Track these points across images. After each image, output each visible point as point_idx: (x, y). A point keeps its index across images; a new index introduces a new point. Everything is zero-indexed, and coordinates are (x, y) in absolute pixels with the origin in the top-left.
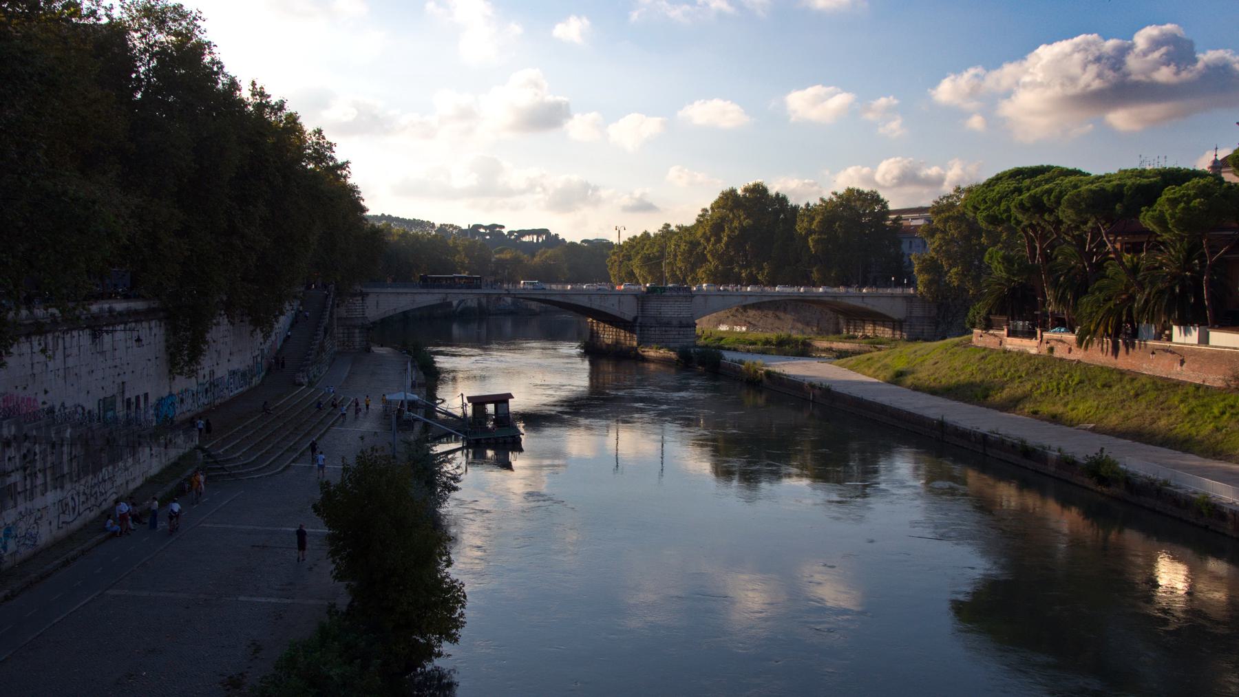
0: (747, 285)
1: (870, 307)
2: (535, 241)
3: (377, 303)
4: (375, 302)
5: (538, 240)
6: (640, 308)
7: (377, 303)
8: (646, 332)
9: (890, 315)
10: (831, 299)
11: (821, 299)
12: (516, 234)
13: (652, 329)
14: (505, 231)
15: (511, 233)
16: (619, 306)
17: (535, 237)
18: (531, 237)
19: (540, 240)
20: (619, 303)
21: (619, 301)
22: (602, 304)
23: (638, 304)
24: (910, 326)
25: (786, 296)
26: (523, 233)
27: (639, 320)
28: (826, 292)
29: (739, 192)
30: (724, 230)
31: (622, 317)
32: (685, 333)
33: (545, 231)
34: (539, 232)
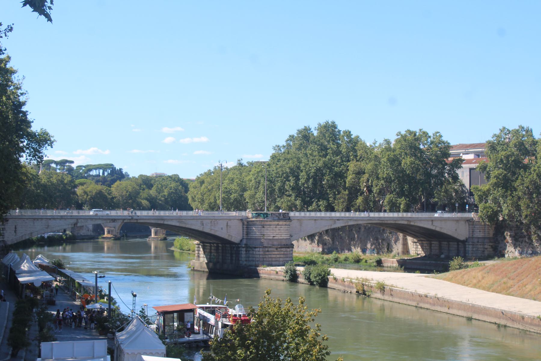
0: (90, 209)
1: (438, 229)
2: (101, 174)
3: (16, 228)
4: (14, 227)
5: (103, 173)
6: (245, 233)
7: (16, 228)
8: (251, 252)
9: (455, 235)
10: (406, 223)
11: (397, 222)
12: (83, 168)
13: (257, 249)
14: (74, 166)
15: (80, 167)
16: (227, 230)
17: (101, 171)
18: (97, 171)
19: (106, 174)
20: (227, 227)
21: (227, 225)
22: (213, 228)
23: (243, 228)
24: (473, 245)
25: (362, 220)
26: (89, 168)
27: (244, 242)
28: (96, 215)
29: (330, 123)
30: (337, 156)
31: (230, 239)
32: (285, 253)
33: (111, 166)
34: (104, 167)
